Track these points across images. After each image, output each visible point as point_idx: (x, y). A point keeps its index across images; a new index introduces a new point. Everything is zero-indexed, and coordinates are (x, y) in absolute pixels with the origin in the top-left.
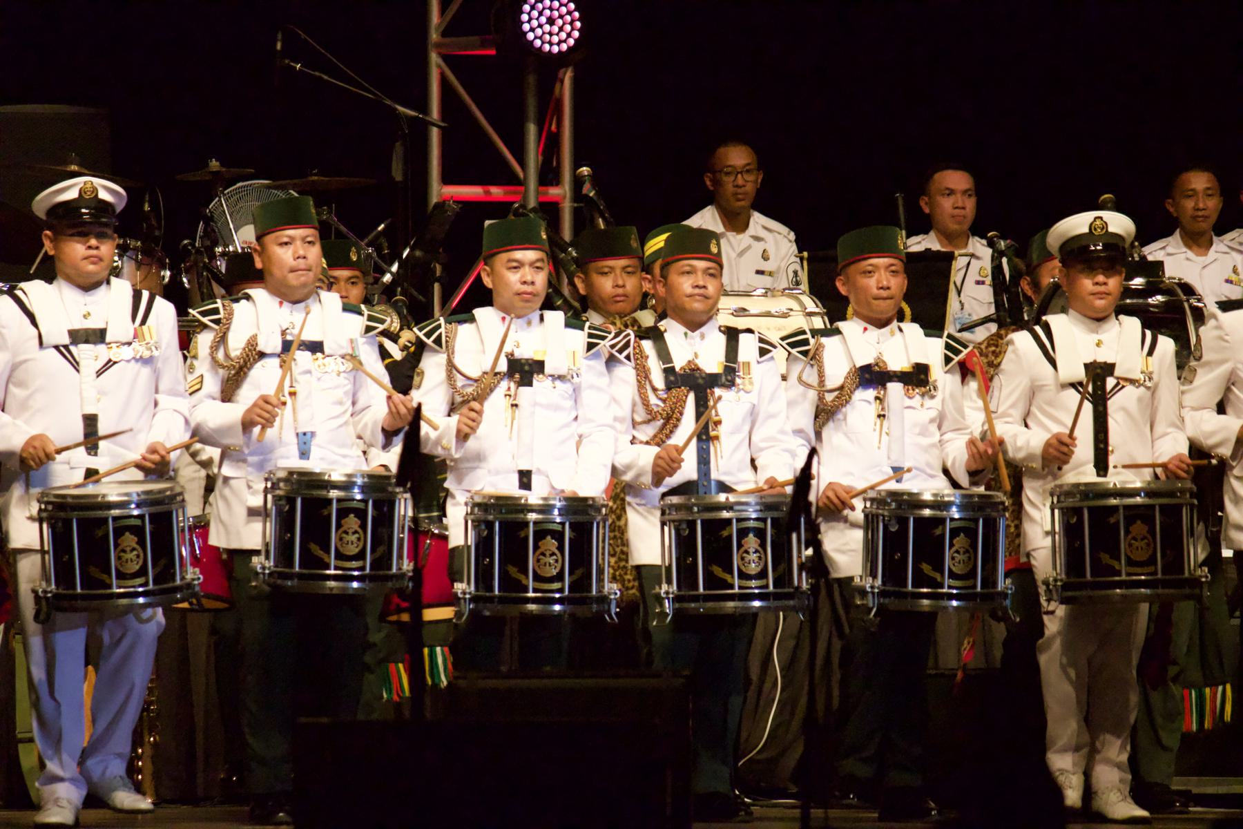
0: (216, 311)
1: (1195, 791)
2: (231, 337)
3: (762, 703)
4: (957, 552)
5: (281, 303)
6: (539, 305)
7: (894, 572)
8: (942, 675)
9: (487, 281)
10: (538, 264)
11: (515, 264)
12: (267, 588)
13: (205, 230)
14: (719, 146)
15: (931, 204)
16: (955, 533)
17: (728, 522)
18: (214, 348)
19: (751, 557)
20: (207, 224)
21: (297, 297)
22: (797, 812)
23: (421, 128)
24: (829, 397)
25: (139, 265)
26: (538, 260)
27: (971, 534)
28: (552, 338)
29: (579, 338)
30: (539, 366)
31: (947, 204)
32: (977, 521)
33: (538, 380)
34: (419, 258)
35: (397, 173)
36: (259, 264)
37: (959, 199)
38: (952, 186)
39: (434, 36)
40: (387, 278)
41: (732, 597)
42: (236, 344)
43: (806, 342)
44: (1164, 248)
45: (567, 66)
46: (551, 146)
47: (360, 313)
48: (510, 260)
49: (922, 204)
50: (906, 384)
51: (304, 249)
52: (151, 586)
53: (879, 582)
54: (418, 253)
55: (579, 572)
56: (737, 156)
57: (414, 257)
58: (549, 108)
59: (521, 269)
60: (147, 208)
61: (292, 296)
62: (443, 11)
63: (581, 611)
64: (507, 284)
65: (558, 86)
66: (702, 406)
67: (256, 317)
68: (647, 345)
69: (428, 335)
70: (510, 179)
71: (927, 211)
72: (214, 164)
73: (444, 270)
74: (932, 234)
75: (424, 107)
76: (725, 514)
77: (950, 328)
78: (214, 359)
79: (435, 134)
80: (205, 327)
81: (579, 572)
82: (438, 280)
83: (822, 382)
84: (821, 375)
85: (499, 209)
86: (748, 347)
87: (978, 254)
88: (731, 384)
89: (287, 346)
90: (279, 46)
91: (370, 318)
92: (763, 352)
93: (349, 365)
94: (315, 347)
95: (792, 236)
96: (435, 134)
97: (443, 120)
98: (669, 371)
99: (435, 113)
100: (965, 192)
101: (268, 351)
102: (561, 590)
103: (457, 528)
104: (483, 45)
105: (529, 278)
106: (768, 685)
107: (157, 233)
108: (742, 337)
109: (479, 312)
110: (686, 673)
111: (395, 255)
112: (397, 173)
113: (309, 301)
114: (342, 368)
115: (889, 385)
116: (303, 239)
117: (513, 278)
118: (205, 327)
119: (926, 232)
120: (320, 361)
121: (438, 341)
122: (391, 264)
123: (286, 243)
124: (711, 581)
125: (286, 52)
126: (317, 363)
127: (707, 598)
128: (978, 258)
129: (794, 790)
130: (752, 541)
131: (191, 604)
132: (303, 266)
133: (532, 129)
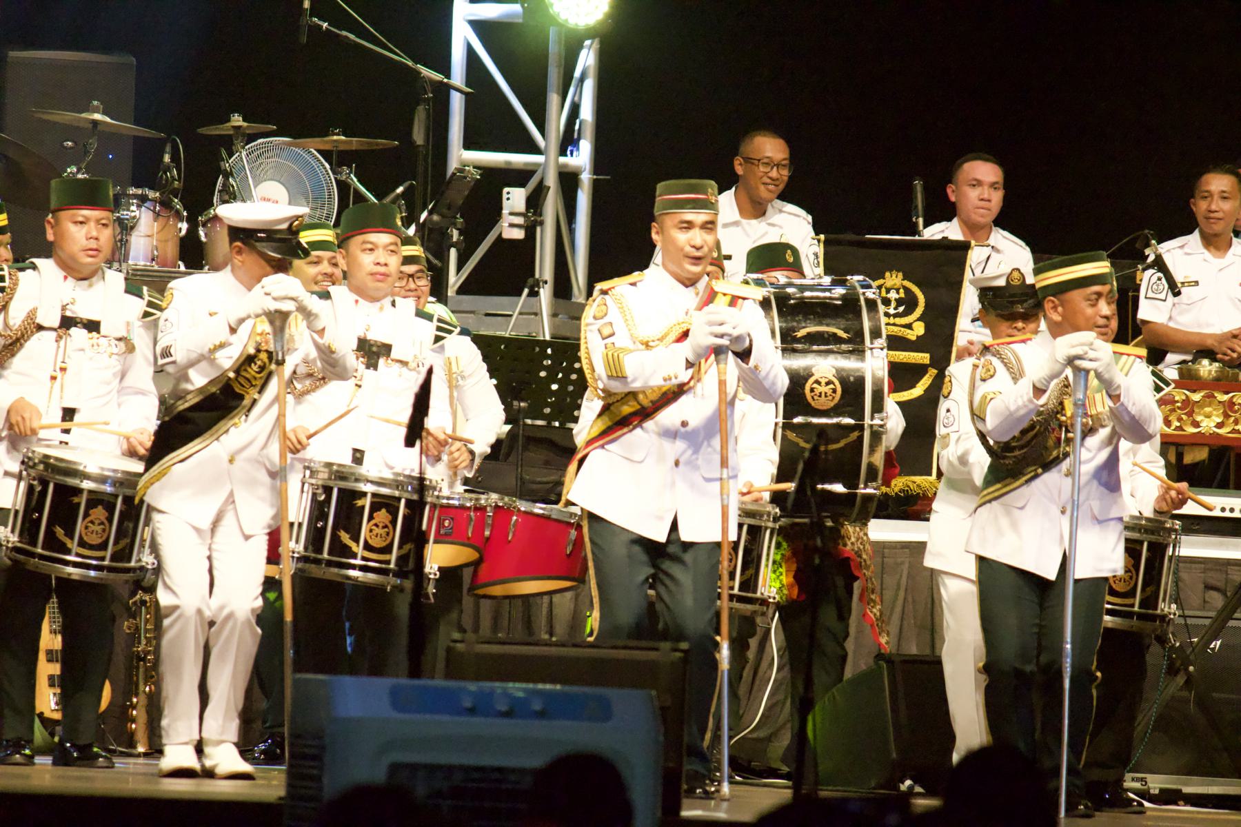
1: (1187, 790)
3: (757, 682)
4: (376, 525)
5: (66, 278)
10: (392, 248)
11: (370, 246)
12: (8, 562)
13: (224, 185)
21: (85, 273)
23: (443, 91)
25: (157, 215)
26: (392, 244)
30: (386, 349)
31: (973, 194)
34: (437, 223)
35: (419, 137)
36: (50, 236)
37: (986, 192)
38: (979, 177)
41: (353, 567)
44: (1182, 247)
47: (140, 296)
48: (364, 242)
49: (949, 191)
51: (98, 231)
54: (435, 218)
57: (431, 220)
60: (167, 158)
61: (80, 273)
64: (360, 265)
71: (953, 199)
72: (237, 120)
74: (955, 220)
79: (457, 103)
81: (124, 542)
85: (519, 177)
87: (999, 247)
89: (67, 323)
94: (93, 326)
95: (810, 218)
96: (457, 103)
99: (458, 76)
100: (993, 185)
101: (45, 324)
105: (382, 261)
106: (764, 665)
112: (419, 137)
113: (94, 279)
114: (116, 350)
116: (98, 221)
119: (949, 219)
120: (94, 341)
123: (81, 223)
125: (314, 11)
126: (92, 342)
127: (330, 564)
128: (998, 251)
129: (785, 769)
132: (95, 246)
133: (553, 99)
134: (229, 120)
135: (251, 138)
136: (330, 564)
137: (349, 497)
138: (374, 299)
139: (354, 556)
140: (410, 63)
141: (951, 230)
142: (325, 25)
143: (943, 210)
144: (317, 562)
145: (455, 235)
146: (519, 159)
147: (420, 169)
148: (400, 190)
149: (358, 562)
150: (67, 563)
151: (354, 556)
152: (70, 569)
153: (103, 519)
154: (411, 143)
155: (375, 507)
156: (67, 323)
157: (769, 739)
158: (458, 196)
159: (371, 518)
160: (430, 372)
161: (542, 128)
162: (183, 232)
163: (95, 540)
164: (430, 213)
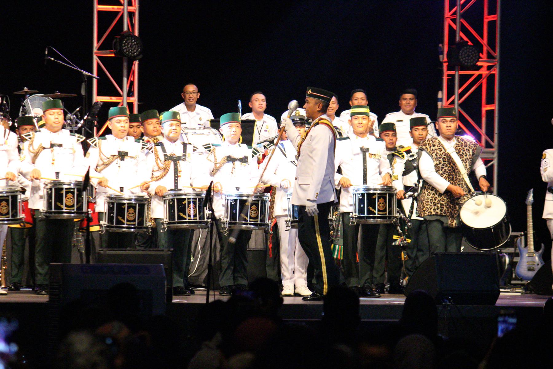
0: (29, 135)
2: (34, 143)
6: (126, 134)
7: (171, 216)
8: (251, 251)
9: (110, 127)
14: (186, 85)
15: (252, 105)
16: (252, 204)
17: (185, 199)
18: (29, 146)
19: (191, 210)
20: (23, 107)
21: (56, 129)
22: (206, 292)
23: (90, 79)
24: (218, 165)
27: (257, 205)
28: (130, 145)
29: (140, 145)
30: (126, 154)
32: (258, 201)
33: (126, 158)
35: (83, 92)
37: (123, 124)
39: (95, 50)
40: (79, 125)
41: (124, 228)
42: (36, 146)
43: (210, 147)
45: (136, 60)
46: (132, 84)
50: (241, 162)
52: (10, 218)
53: (229, 219)
54: (89, 118)
55: (140, 219)
56: (191, 88)
58: (130, 71)
59: (119, 123)
62: (98, 40)
63: (141, 231)
65: (133, 66)
66: (176, 165)
67: (41, 137)
68: (159, 148)
69: (92, 143)
70: (118, 95)
71: (251, 107)
72: (26, 89)
73: (98, 122)
75: (92, 73)
76: (183, 197)
77: (254, 145)
78: (29, 150)
79: (95, 81)
80: (26, 140)
81: (140, 219)
82: (95, 126)
83: (216, 160)
84: (215, 156)
85: (115, 104)
86: (189, 148)
88: (184, 160)
89: (52, 146)
90: (46, 53)
91: (79, 137)
92: (194, 150)
93: (72, 151)
96: (95, 81)
97: (98, 76)
98: (165, 155)
99: (95, 74)
102: (134, 225)
103: (101, 206)
104: (110, 53)
106: (196, 253)
107: (8, 110)
108: (188, 145)
109: (107, 136)
110: (172, 250)
111: (82, 118)
112: (83, 92)
115: (236, 162)
116: (58, 113)
117: (118, 126)
118: (26, 140)
121: (95, 145)
122: (80, 120)
124: (180, 218)
125: (48, 55)
127: (178, 223)
129: (204, 285)
130: (192, 205)
131: (21, 226)
133: (125, 79)
134: (23, 89)
135: (31, 95)
136: (116, 227)
137: (120, 206)
138: (122, 138)
139: (124, 224)
140: (80, 70)
141: (249, 116)
142: (52, 59)
143: (247, 109)
144: (174, 223)
145: (96, 123)
146: (114, 99)
147: (84, 104)
148: (78, 109)
149: (187, 220)
150: (124, 228)
151: (186, 219)
152: (124, 230)
153: (133, 212)
154: (81, 94)
155: (379, 198)
156: (52, 146)
157: (198, 276)
158: (96, 110)
159: (378, 201)
160: (89, 167)
161: (122, 90)
162: (10, 125)
163: (132, 219)
164: (88, 116)
